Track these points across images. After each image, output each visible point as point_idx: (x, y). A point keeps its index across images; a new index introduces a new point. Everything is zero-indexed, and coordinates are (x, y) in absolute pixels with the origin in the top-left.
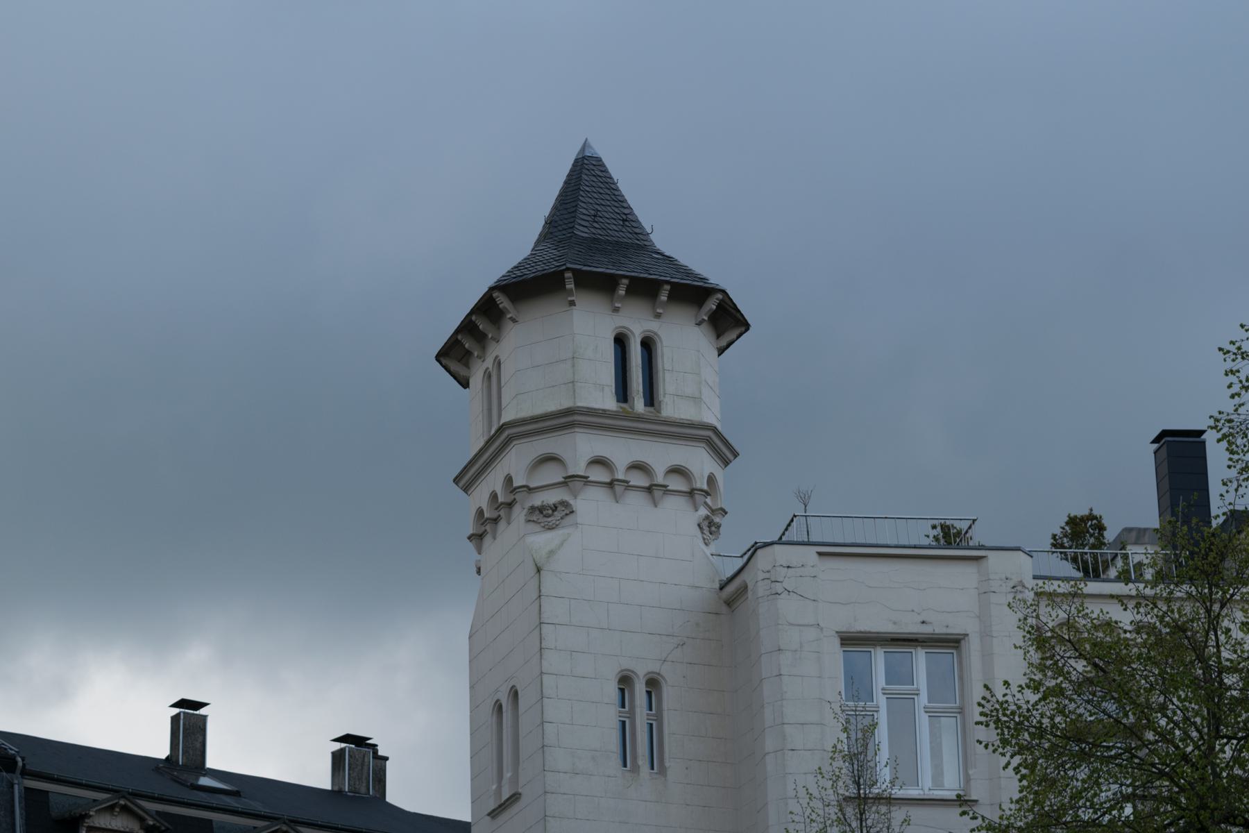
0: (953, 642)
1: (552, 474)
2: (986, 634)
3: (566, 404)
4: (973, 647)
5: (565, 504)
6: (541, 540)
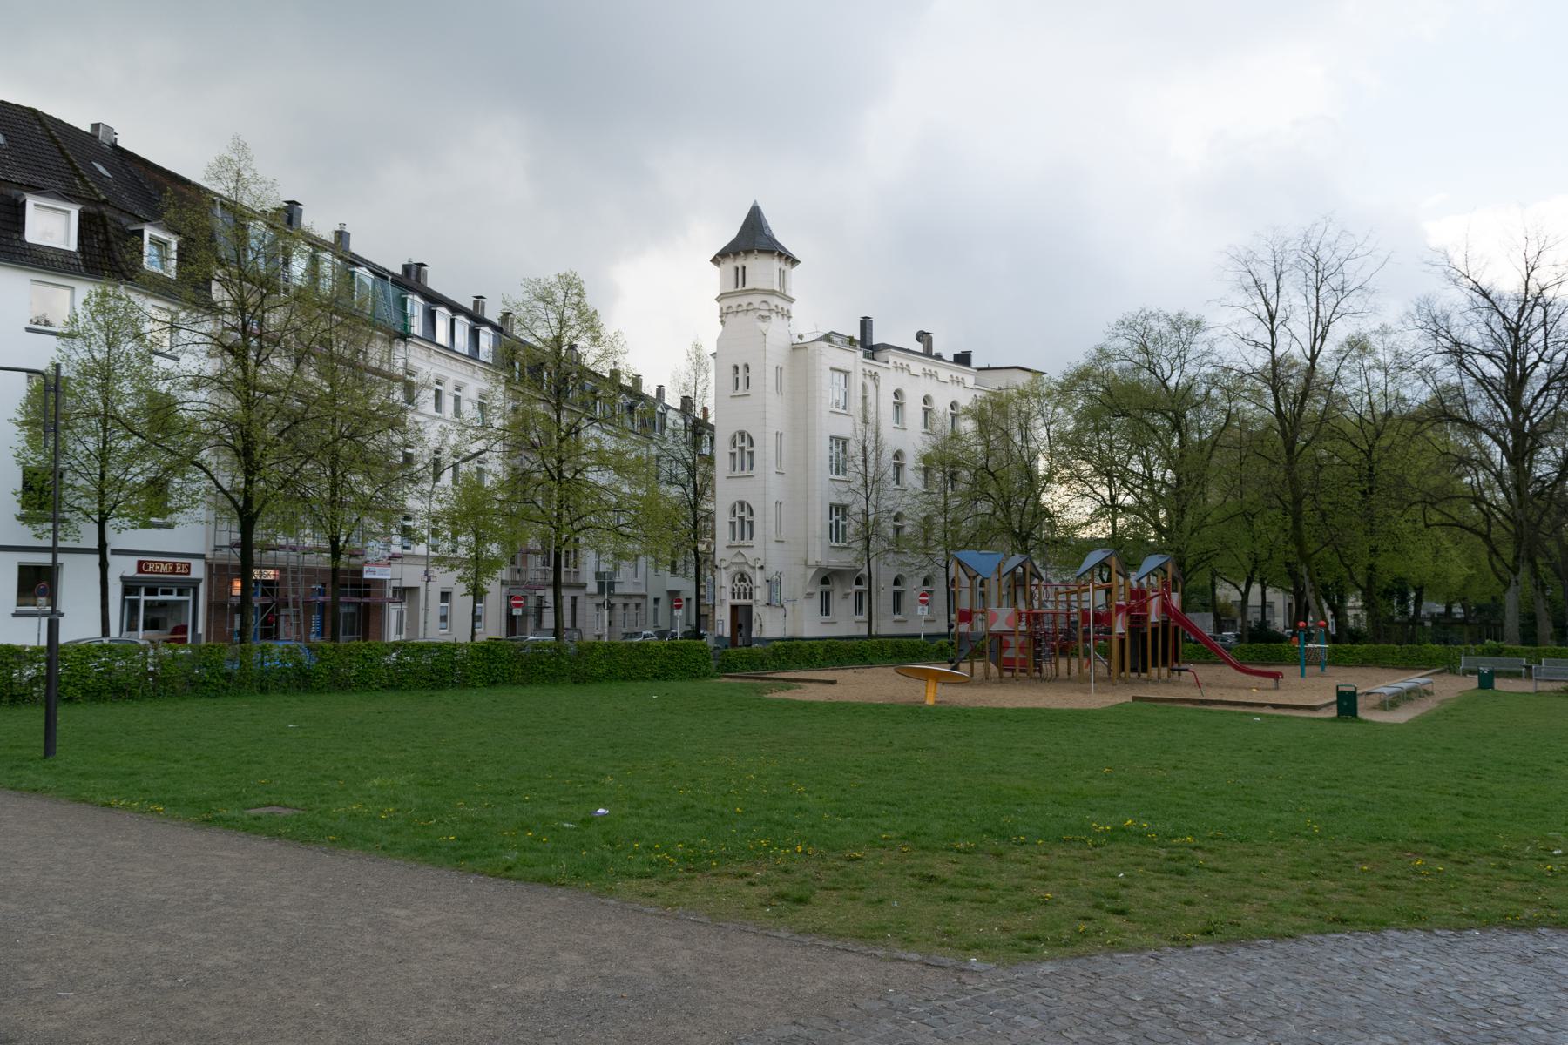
0: (847, 373)
1: (765, 306)
2: (855, 372)
3: (770, 288)
4: (852, 376)
6: (762, 325)
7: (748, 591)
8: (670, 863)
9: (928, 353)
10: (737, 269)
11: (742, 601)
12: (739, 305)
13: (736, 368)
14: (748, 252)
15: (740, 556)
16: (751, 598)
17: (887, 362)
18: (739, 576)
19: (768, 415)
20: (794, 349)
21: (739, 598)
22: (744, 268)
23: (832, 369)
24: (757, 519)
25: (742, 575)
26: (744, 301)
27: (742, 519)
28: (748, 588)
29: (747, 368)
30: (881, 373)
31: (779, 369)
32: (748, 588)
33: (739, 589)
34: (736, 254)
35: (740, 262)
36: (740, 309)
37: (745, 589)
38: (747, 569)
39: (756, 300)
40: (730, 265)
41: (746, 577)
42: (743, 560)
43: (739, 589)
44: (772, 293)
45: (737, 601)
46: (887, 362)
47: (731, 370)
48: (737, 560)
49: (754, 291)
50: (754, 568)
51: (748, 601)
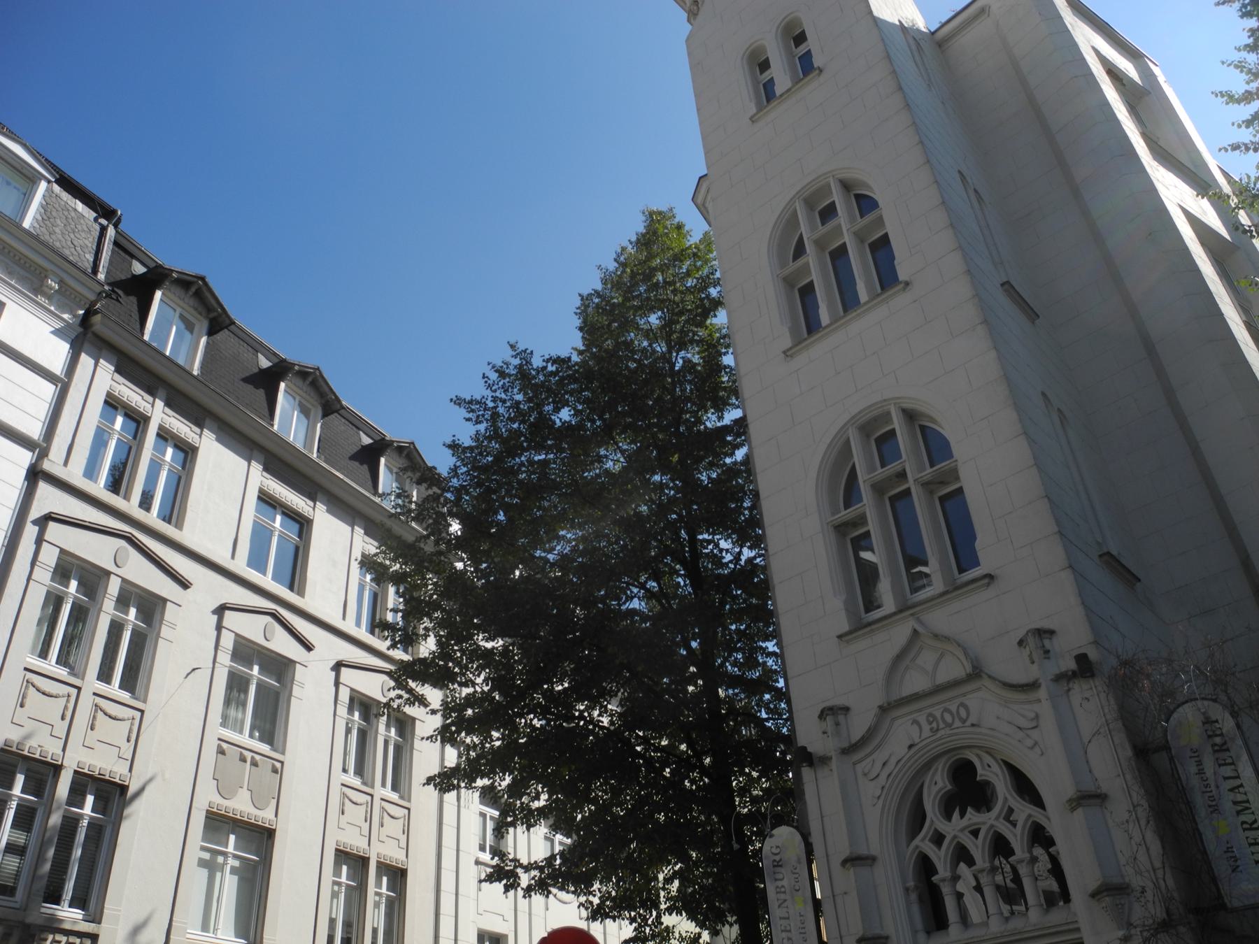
18: (938, 783)
25: (963, 772)
41: (991, 773)
42: (953, 669)
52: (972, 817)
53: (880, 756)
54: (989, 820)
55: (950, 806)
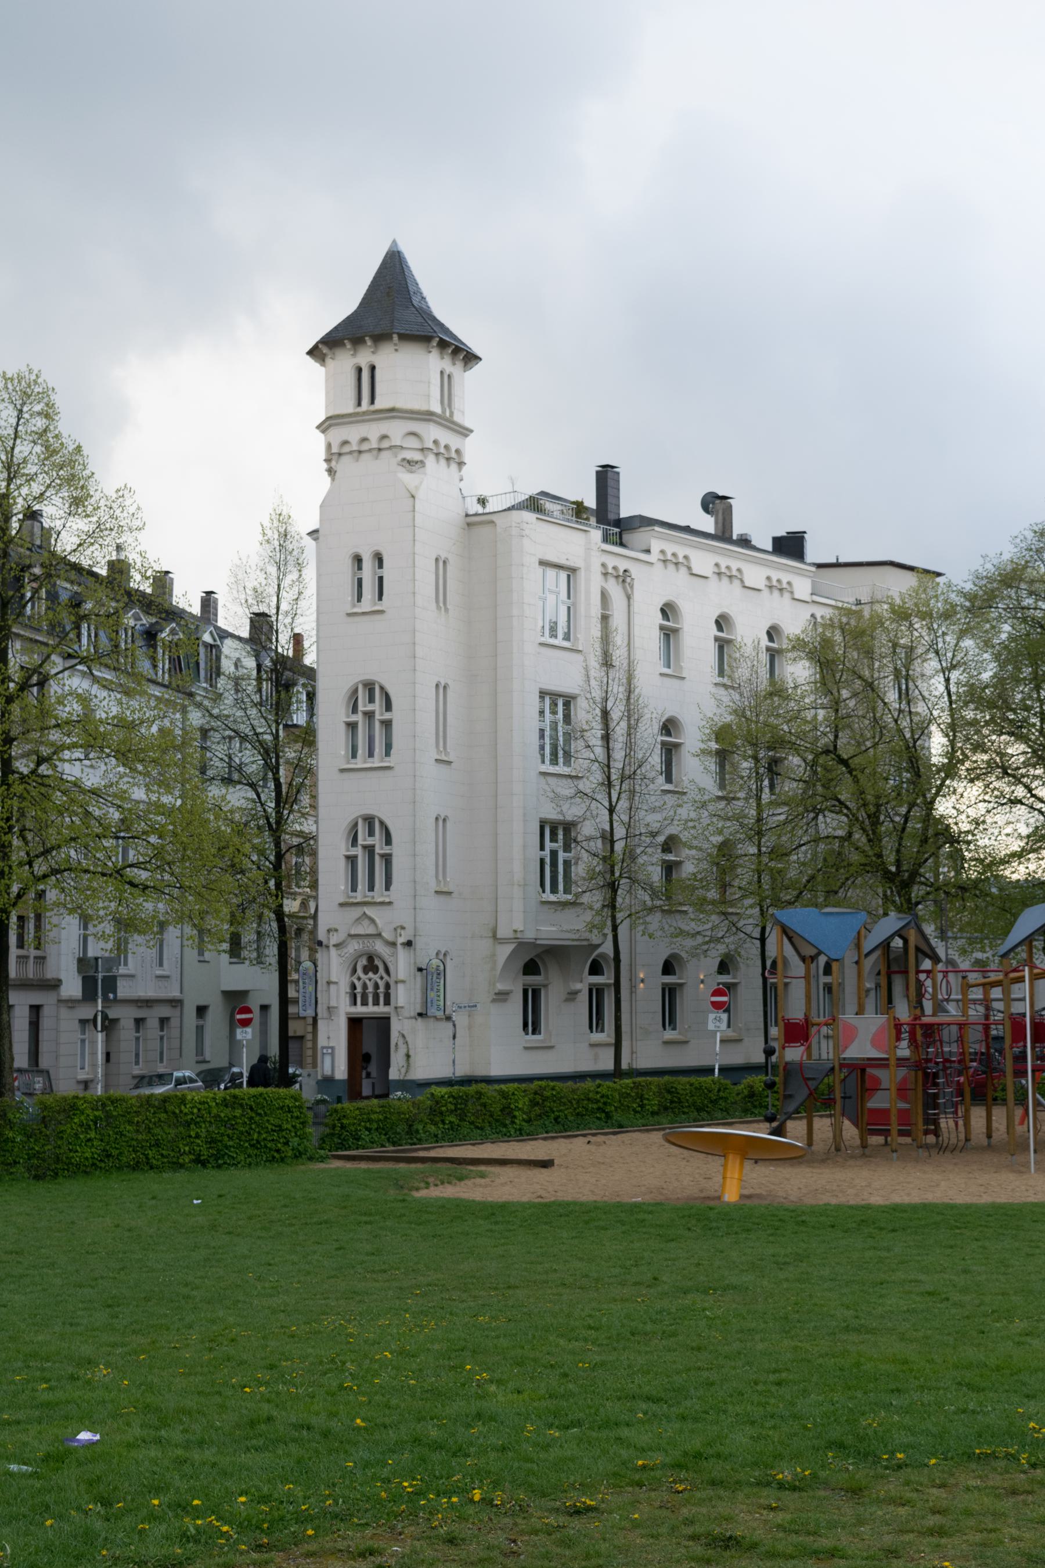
0: (571, 571)
1: (413, 442)
2: (588, 569)
4: (582, 575)
5: (422, 462)
6: (408, 479)
7: (382, 989)
8: (223, 1535)
9: (724, 534)
10: (360, 370)
11: (371, 1009)
12: (384, 437)
13: (358, 560)
14: (380, 338)
15: (366, 922)
16: (387, 1002)
17: (648, 551)
18: (363, 962)
19: (420, 652)
20: (469, 524)
21: (365, 1003)
22: (373, 368)
23: (543, 563)
24: (399, 852)
25: (371, 959)
26: (373, 431)
27: (370, 850)
28: (381, 984)
29: (379, 559)
30: (635, 570)
31: (441, 563)
32: (381, 984)
33: (365, 986)
34: (358, 341)
35: (364, 357)
36: (365, 446)
37: (376, 986)
38: (379, 947)
39: (396, 430)
40: (345, 362)
41: (377, 962)
42: (371, 930)
43: (365, 986)
44: (427, 416)
45: (360, 1010)
46: (648, 551)
47: (348, 564)
48: (360, 930)
49: (392, 413)
50: (393, 944)
51: (381, 1009)
52: (371, 975)
53: (345, 950)
54: (375, 977)
55: (366, 970)
